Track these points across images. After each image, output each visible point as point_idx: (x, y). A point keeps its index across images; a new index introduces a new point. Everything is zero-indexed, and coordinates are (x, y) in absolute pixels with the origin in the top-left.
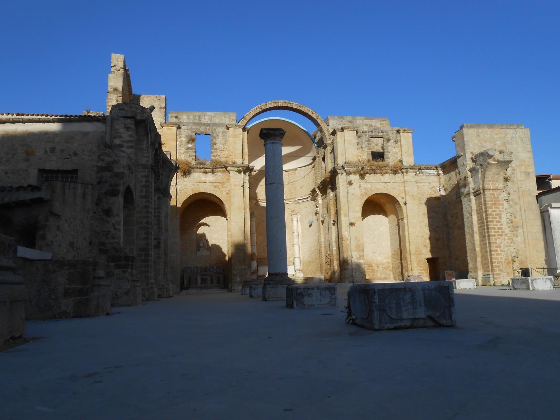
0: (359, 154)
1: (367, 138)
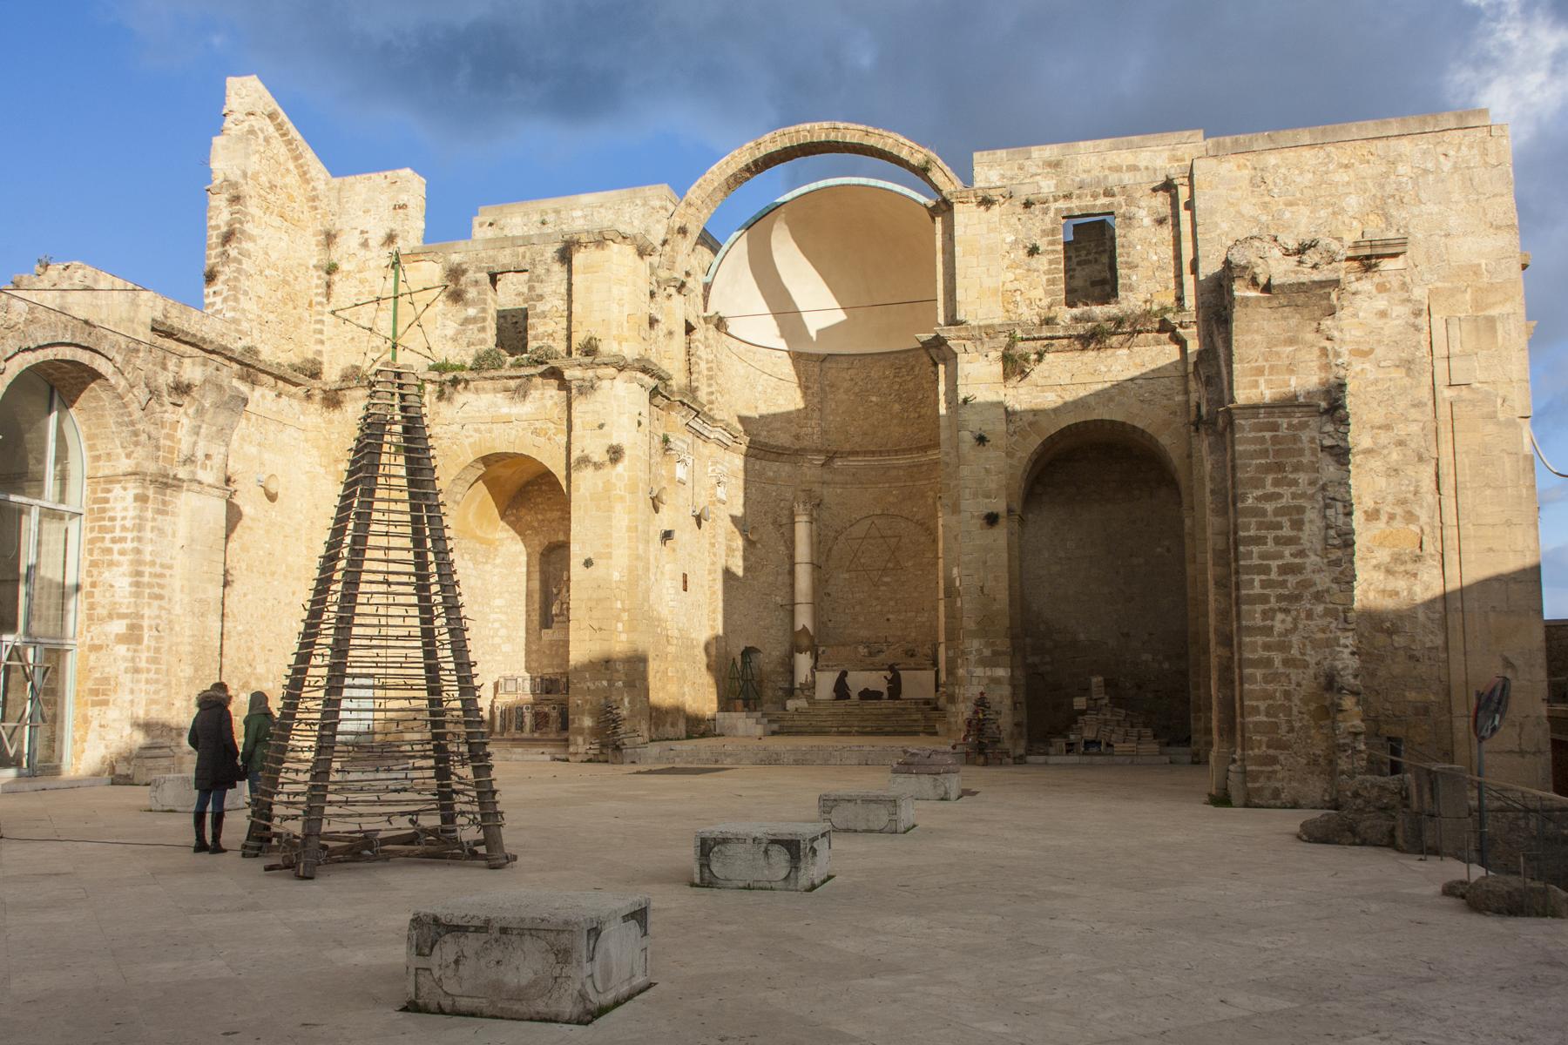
0: (1017, 285)
1: (1047, 219)
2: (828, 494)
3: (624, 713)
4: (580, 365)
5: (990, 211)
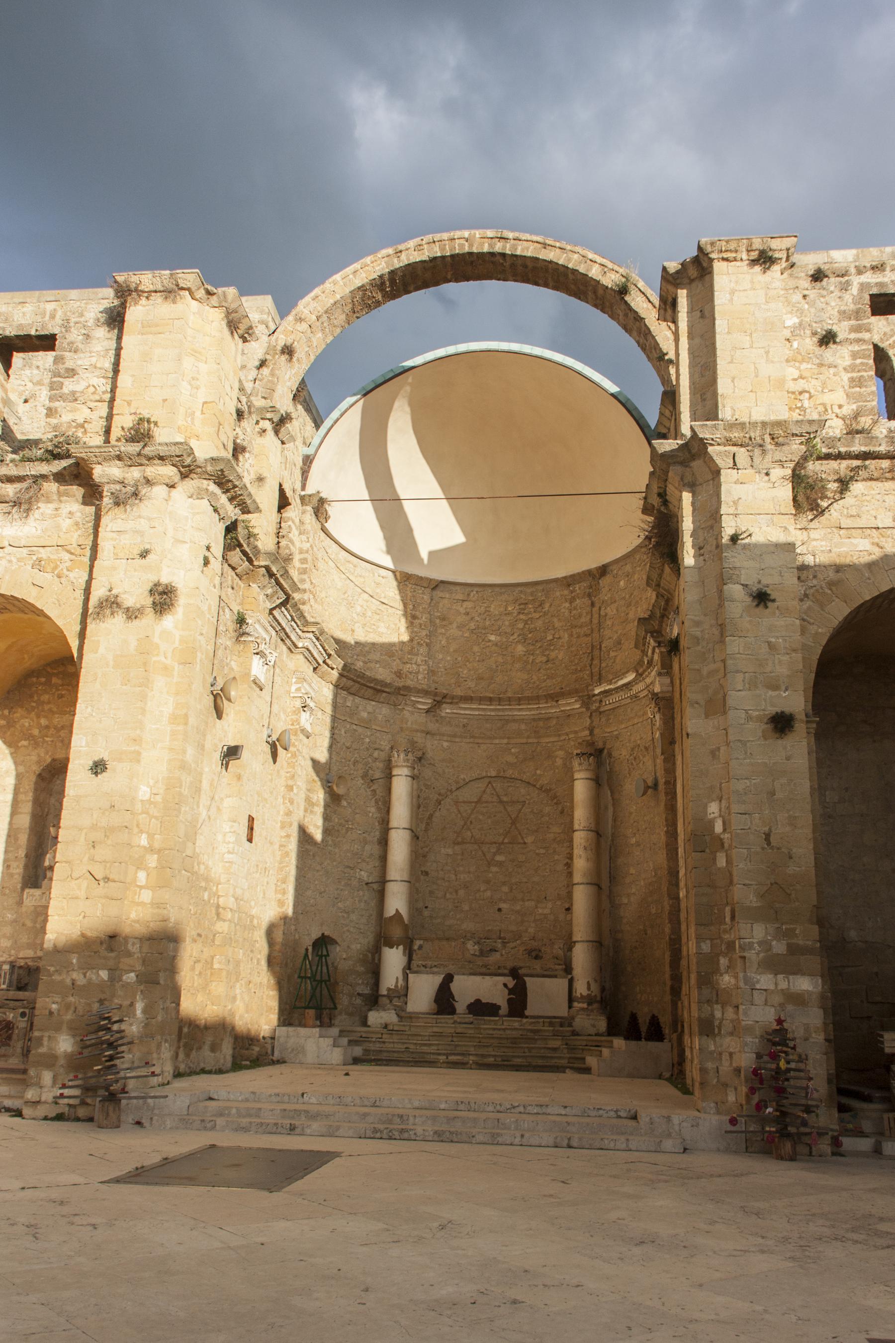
0: (802, 385)
1: (848, 297)
2: (431, 746)
3: (133, 1028)
4: (119, 458)
5: (769, 273)
